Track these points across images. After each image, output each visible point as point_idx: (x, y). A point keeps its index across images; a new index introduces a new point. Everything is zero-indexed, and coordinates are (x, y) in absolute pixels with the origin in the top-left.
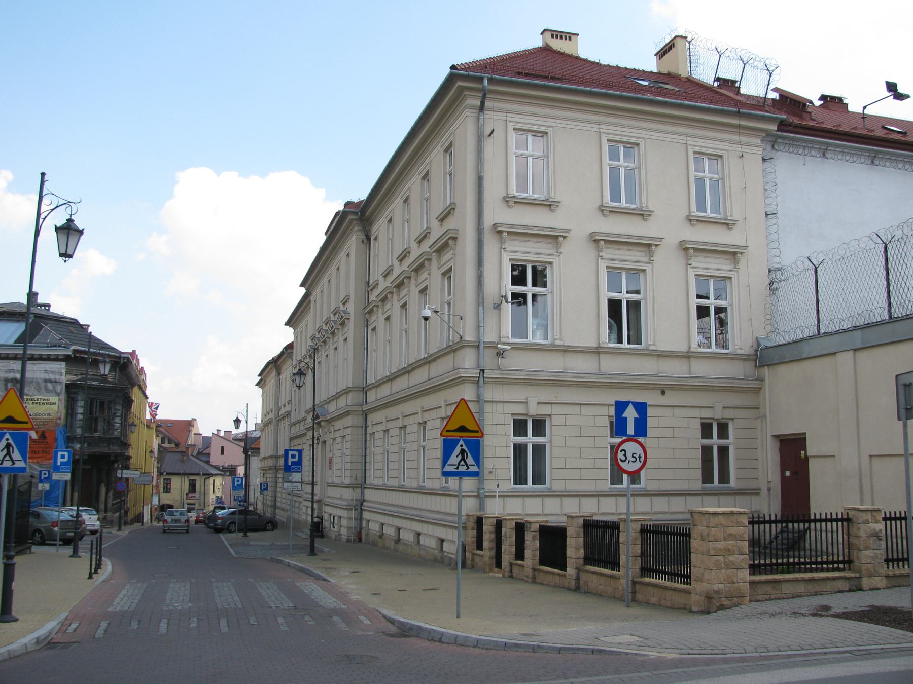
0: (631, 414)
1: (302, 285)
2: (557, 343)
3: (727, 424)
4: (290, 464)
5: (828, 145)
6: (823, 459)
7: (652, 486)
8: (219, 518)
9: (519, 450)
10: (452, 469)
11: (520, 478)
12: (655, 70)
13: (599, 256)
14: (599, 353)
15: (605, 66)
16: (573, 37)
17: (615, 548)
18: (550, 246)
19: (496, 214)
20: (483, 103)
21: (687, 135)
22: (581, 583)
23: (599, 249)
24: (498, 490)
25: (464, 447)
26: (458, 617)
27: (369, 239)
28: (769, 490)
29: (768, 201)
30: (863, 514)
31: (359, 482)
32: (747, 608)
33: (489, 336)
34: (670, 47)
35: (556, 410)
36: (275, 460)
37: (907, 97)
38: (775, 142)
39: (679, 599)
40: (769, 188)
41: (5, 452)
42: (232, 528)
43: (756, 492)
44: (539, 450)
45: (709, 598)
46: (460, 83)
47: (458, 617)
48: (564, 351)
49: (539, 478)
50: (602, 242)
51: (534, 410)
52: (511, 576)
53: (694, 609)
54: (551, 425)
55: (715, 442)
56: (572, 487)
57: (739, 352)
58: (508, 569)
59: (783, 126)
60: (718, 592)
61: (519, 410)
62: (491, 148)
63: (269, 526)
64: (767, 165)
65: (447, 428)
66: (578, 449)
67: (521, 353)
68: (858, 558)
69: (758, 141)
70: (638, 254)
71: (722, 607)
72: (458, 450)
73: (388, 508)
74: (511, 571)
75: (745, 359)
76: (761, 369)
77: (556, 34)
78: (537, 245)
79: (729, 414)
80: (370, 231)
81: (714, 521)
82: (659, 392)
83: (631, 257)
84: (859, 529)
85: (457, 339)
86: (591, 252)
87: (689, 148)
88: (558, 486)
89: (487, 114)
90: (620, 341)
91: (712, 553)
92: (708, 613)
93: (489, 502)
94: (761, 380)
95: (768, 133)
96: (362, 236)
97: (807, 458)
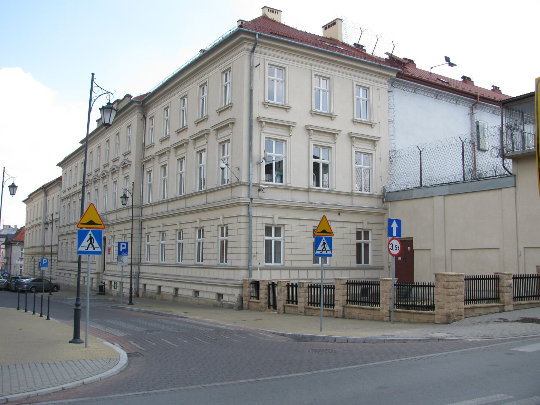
0: (394, 225)
1: (81, 142)
2: (289, 185)
3: (368, 232)
4: (121, 250)
5: (418, 86)
6: (422, 251)
7: (333, 265)
8: (25, 284)
9: (268, 244)
10: (84, 249)
11: (268, 259)
12: (321, 35)
13: (310, 138)
14: (309, 191)
15: (299, 31)
16: (279, 12)
17: (377, 295)
18: (285, 131)
19: (259, 111)
20: (254, 48)
21: (353, 75)
22: (346, 313)
23: (310, 135)
24: (259, 266)
25: (92, 236)
26: (321, 331)
27: (145, 118)
28: (389, 267)
29: (390, 114)
30: (506, 276)
31: (137, 262)
32: (465, 321)
33: (255, 180)
34: (332, 24)
35: (287, 222)
36: (43, 248)
37: (455, 65)
38: (393, 83)
39: (430, 318)
40: (391, 106)
41: (89, 242)
42: (34, 290)
43: (381, 268)
44: (278, 243)
45: (448, 316)
46: (243, 36)
47: (321, 331)
48: (292, 190)
49: (278, 260)
50: (312, 131)
51: (277, 222)
52: (285, 313)
53: (437, 322)
54: (285, 230)
55: (362, 241)
56: (295, 264)
57: (375, 194)
58: (282, 309)
59: (399, 75)
60: (453, 313)
61: (269, 221)
62: (257, 73)
63: (55, 289)
64: (390, 95)
65: (81, 222)
66: (297, 242)
67: (274, 190)
68: (503, 296)
69: (386, 81)
70: (328, 138)
71: (454, 321)
72: (88, 237)
73: (157, 276)
74: (284, 310)
75: (378, 198)
76: (387, 203)
77: (271, 10)
78: (279, 130)
79: (370, 226)
80: (146, 113)
81: (451, 278)
82: (337, 214)
83: (326, 140)
84: (503, 283)
85: (236, 181)
86: (306, 137)
87: (354, 82)
88: (287, 264)
89: (255, 55)
90: (318, 185)
91: (451, 294)
92: (448, 323)
93: (254, 272)
94: (386, 209)
95: (391, 78)
96: (142, 116)
97: (412, 250)
